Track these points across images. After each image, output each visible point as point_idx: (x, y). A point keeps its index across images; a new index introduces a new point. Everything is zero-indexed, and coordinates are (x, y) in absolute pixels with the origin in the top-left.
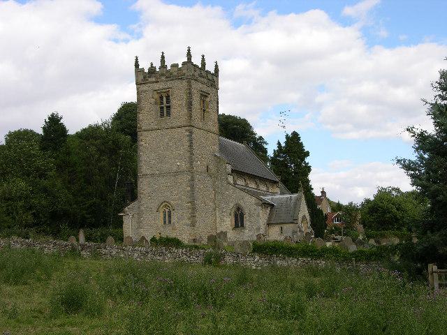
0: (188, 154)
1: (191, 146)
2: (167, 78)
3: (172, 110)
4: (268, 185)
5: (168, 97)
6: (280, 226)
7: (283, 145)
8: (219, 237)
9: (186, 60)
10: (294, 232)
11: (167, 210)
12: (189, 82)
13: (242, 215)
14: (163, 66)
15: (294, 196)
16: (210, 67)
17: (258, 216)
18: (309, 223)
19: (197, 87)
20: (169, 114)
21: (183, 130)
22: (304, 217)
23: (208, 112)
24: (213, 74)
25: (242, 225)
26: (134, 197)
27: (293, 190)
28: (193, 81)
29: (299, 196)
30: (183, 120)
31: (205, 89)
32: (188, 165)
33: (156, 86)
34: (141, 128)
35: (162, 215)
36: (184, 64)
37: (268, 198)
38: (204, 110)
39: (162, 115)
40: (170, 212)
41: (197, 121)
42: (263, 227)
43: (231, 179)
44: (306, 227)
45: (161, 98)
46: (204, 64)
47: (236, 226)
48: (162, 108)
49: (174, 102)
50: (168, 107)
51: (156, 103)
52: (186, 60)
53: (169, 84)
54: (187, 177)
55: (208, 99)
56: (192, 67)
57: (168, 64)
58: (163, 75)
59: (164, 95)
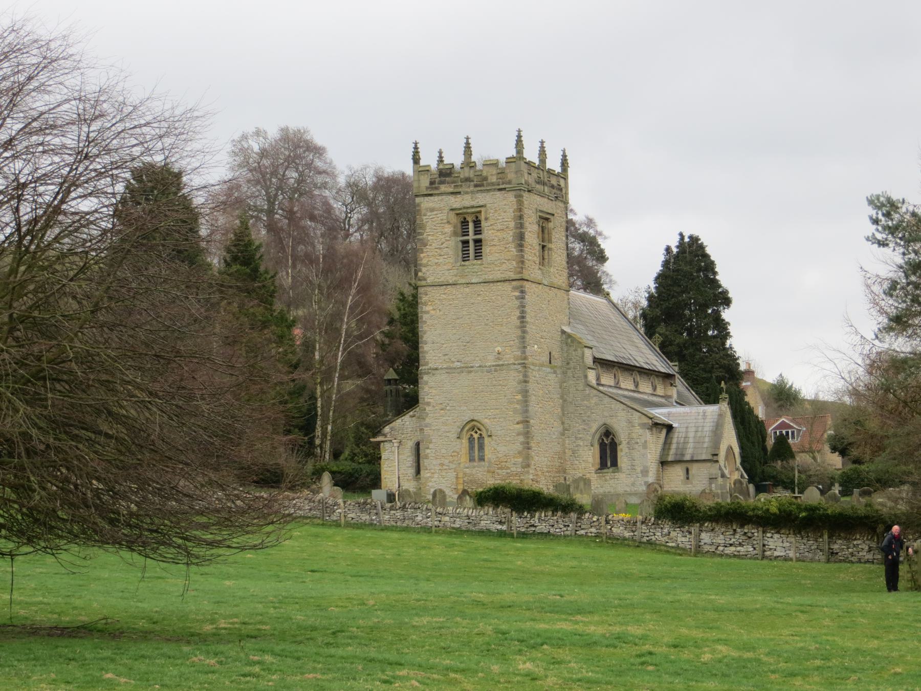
0: (519, 332)
1: (522, 318)
2: (476, 186)
3: (486, 250)
4: (638, 378)
5: (477, 223)
6: (684, 466)
7: (675, 250)
8: (577, 488)
9: (513, 152)
10: (712, 479)
11: (476, 436)
12: (519, 197)
13: (614, 446)
14: (468, 163)
15: (712, 409)
16: (554, 164)
17: (645, 445)
18: (738, 460)
19: (534, 203)
20: (478, 255)
21: (507, 287)
22: (730, 448)
23: (550, 249)
24: (558, 175)
25: (615, 464)
26: (411, 402)
27: (709, 398)
28: (526, 195)
29: (720, 410)
30: (508, 269)
31: (547, 205)
32: (519, 353)
33: (457, 202)
34: (425, 279)
35: (465, 442)
36: (509, 161)
37: (660, 414)
38: (543, 247)
39: (465, 258)
40: (481, 437)
41: (533, 271)
42: (653, 467)
43: (592, 376)
44: (735, 473)
45: (465, 223)
46: (542, 153)
47: (603, 465)
48: (465, 243)
49: (488, 234)
50: (478, 242)
51: (455, 234)
52: (513, 152)
53: (481, 199)
54: (512, 378)
55: (551, 225)
56: (524, 167)
57: (477, 157)
58: (468, 180)
59: (470, 219)
